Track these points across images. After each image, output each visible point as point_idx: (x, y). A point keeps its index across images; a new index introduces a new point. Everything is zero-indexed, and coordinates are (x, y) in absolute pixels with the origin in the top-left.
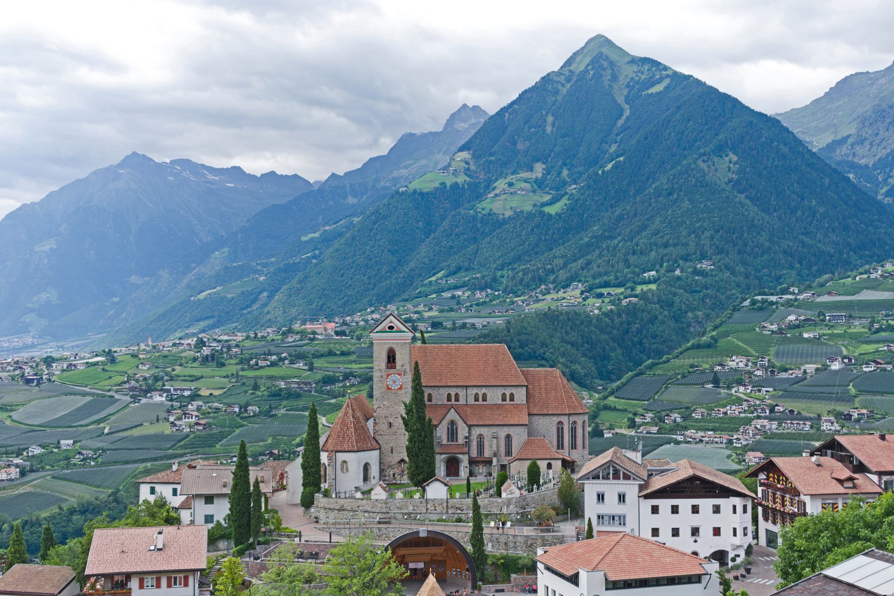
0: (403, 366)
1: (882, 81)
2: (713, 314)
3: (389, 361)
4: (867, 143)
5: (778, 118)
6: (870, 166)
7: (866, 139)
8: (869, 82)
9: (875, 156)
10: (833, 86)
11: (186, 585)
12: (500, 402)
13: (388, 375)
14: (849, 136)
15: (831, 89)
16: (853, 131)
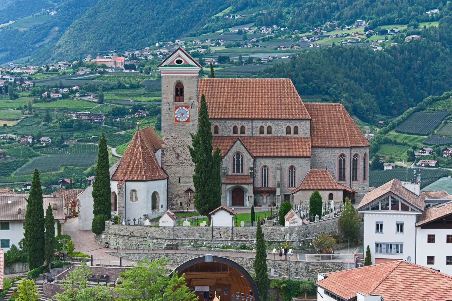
0: (190, 99)
12: (284, 135)
13: (176, 108)
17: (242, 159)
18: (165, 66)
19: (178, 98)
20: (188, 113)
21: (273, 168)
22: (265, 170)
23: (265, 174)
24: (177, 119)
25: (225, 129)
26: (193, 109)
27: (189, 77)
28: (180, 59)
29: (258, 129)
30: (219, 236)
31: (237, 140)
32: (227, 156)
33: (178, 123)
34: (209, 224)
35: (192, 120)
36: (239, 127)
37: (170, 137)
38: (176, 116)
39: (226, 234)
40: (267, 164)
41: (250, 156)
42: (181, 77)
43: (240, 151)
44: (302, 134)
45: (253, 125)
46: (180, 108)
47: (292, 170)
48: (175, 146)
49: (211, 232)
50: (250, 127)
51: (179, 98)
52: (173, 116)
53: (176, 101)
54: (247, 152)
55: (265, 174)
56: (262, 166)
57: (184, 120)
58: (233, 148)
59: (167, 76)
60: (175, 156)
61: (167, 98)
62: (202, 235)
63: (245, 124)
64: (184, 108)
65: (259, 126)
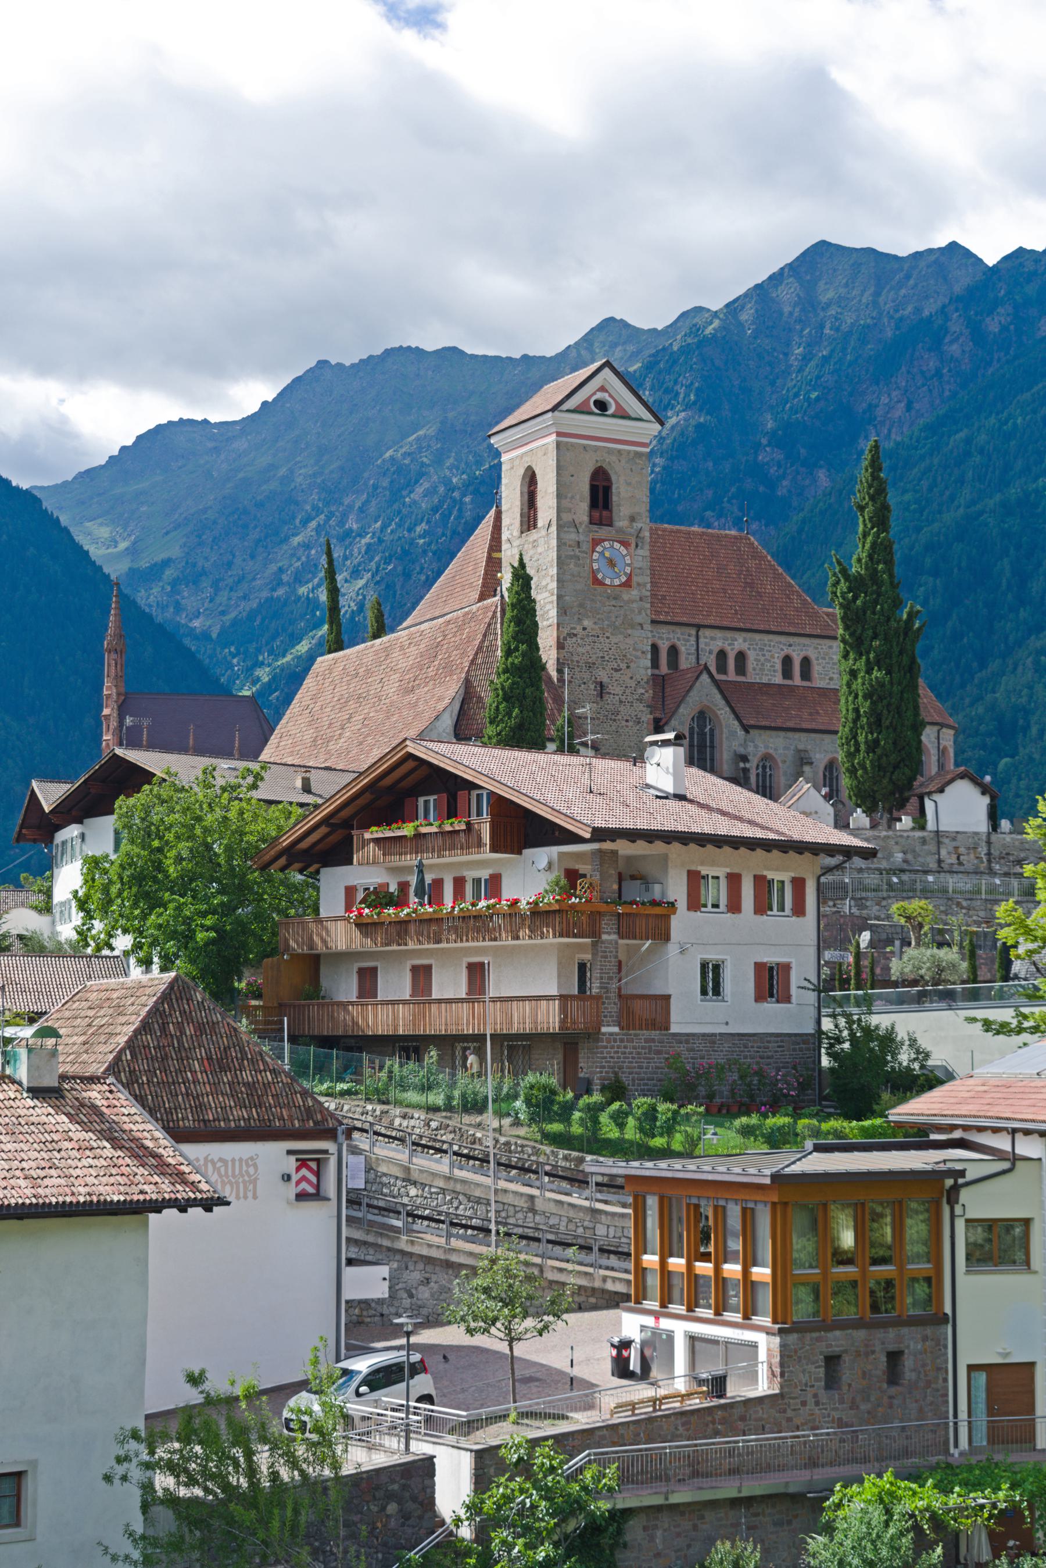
0: (632, 519)
1: (241, 444)
3: (594, 504)
4: (206, 583)
5: (35, 492)
6: (214, 636)
7: (204, 573)
8: (210, 445)
9: (223, 613)
10: (129, 442)
12: (778, 679)
13: (596, 542)
14: (166, 563)
15: (123, 449)
16: (175, 551)
17: (712, 730)
18: (568, 411)
19: (596, 514)
20: (628, 560)
21: (788, 763)
22: (764, 767)
23: (764, 781)
24: (600, 576)
27: (629, 452)
30: (953, 860)
31: (701, 673)
32: (676, 717)
34: (920, 821)
35: (639, 584)
36: (664, 647)
38: (595, 566)
39: (972, 856)
40: (771, 751)
41: (736, 723)
42: (610, 451)
44: (821, 679)
45: (701, 646)
46: (607, 544)
47: (831, 773)
48: (594, 657)
49: (934, 849)
50: (693, 649)
51: (601, 516)
53: (591, 523)
54: (728, 709)
55: (764, 781)
56: (760, 753)
57: (617, 582)
58: (691, 694)
62: (910, 857)
64: (617, 545)
65: (716, 650)
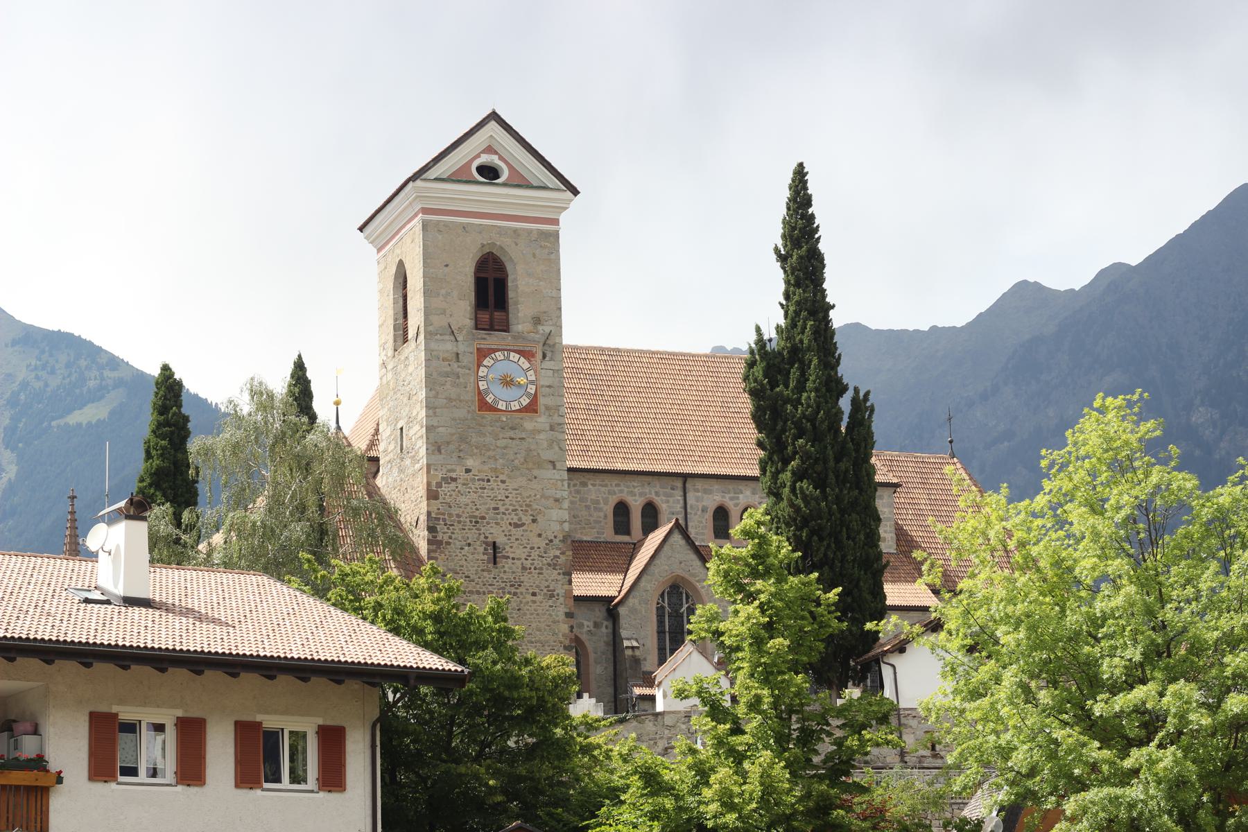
2: (1050, 552)
11: (333, 779)
13: (482, 354)
19: (485, 316)
24: (489, 399)
25: (585, 513)
26: (547, 364)
27: (530, 232)
28: (493, 160)
29: (709, 515)
33: (489, 416)
35: (547, 408)
37: (459, 472)
43: (687, 576)
45: (689, 502)
48: (483, 508)
51: (491, 319)
52: (470, 387)
53: (477, 328)
59: (446, 224)
60: (480, 555)
61: (444, 312)
63: (657, 494)
64: (514, 357)
